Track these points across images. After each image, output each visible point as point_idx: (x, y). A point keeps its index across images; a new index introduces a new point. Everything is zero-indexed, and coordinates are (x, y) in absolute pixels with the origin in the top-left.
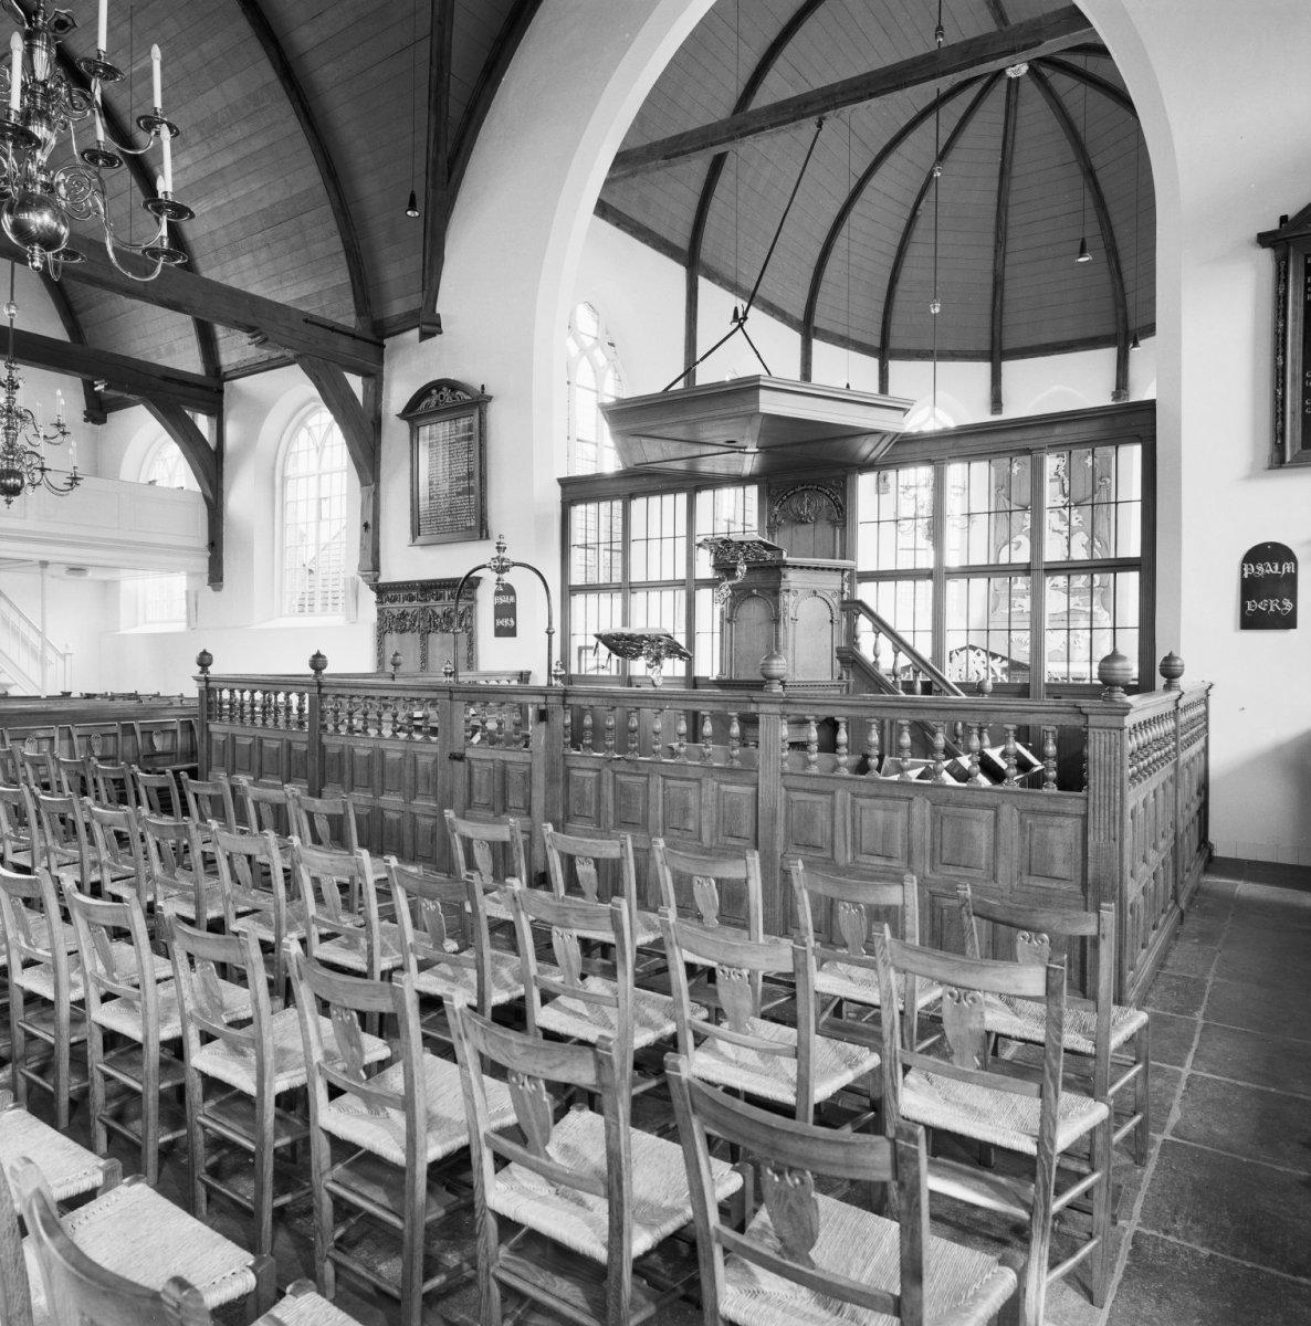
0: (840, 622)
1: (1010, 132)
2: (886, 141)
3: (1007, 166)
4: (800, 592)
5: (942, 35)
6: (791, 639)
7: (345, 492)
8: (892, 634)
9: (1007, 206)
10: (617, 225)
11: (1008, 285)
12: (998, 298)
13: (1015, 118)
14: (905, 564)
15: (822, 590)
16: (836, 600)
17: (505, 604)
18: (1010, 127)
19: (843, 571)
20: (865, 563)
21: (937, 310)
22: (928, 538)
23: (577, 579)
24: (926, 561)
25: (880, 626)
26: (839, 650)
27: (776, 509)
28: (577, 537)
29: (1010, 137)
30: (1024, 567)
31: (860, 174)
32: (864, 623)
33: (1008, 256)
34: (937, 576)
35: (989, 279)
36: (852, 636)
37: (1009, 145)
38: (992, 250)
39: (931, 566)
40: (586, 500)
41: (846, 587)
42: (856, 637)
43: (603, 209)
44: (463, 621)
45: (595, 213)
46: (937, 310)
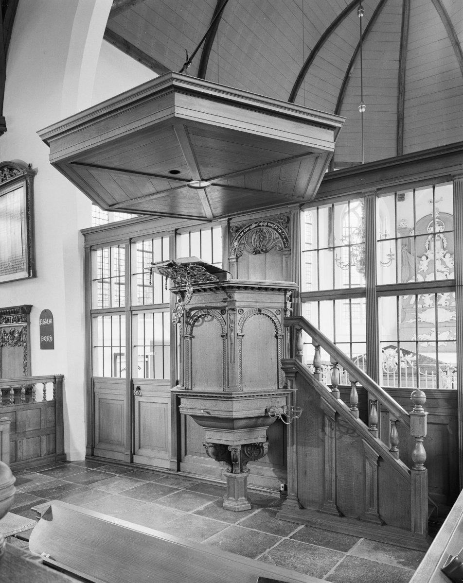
0: (284, 337)
1: (406, 20)
2: (328, 25)
3: (405, 43)
4: (245, 310)
5: (362, 12)
6: (237, 353)
7: (352, 287)
8: (331, 348)
9: (405, 70)
10: (140, 60)
11: (406, 121)
12: (401, 129)
13: (409, 10)
14: (342, 284)
15: (267, 309)
16: (279, 317)
17: (46, 325)
18: (406, 16)
19: (286, 290)
20: (307, 285)
21: (364, 110)
22: (360, 272)
23: (97, 305)
24: (360, 281)
25: (320, 341)
26: (284, 362)
27: (236, 243)
28: (97, 273)
29: (406, 23)
30: (449, 284)
31: (312, 47)
32: (305, 338)
33: (406, 103)
34: (373, 293)
35: (395, 118)
36: (294, 350)
37: (406, 28)
38: (396, 99)
39: (452, 277)
40: (102, 245)
41: (289, 305)
42: (299, 350)
43: (110, 35)
44: (21, 340)
45: (104, 38)
46: (364, 110)
